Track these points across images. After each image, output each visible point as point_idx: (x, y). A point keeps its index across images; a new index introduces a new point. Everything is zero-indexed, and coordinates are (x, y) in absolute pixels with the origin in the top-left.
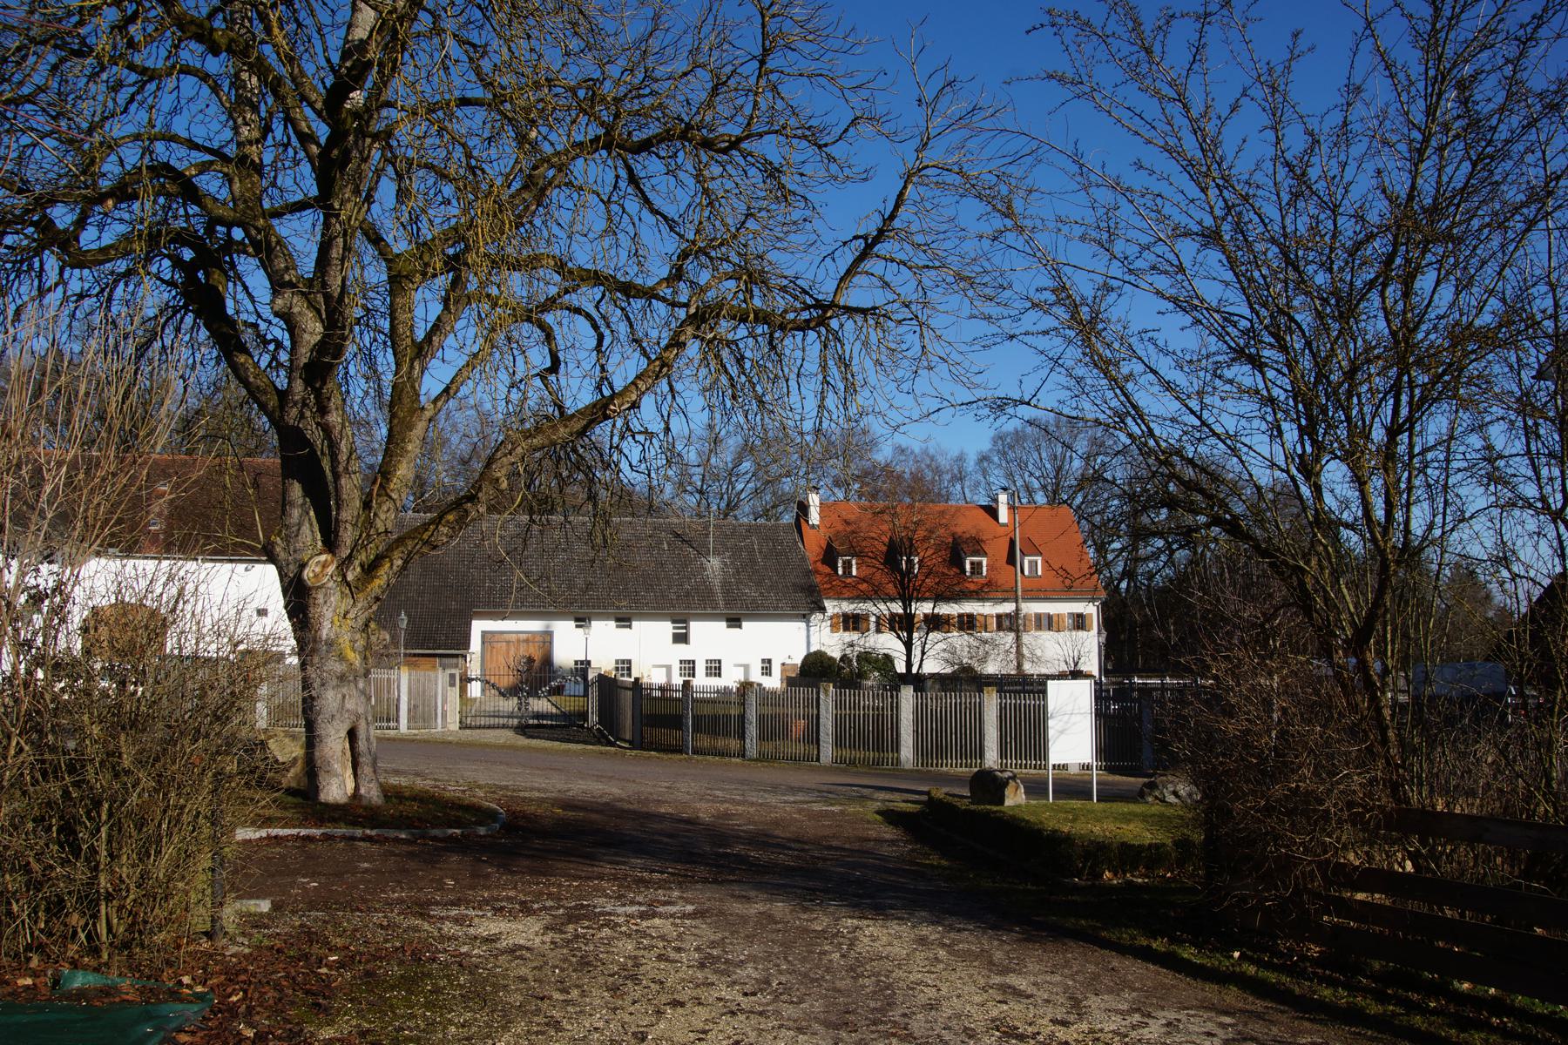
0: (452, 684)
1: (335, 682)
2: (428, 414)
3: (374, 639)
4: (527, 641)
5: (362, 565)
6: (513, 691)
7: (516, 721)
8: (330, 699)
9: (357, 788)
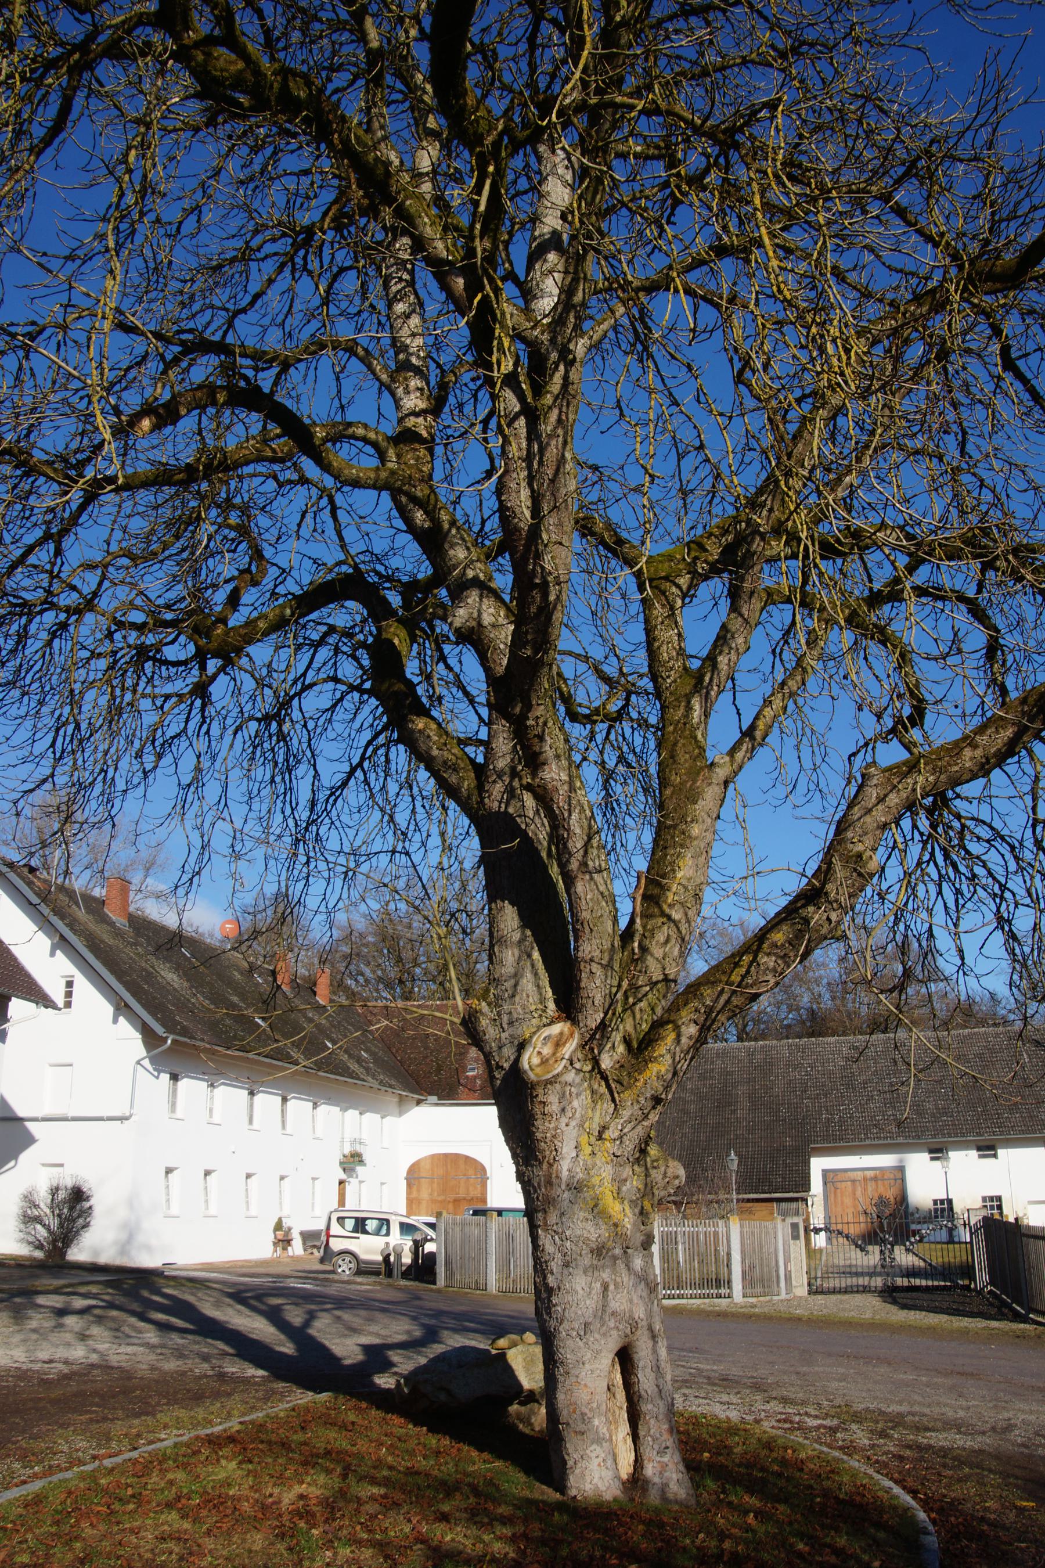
0: (796, 1237)
1: (587, 1260)
2: (721, 773)
3: (656, 1175)
4: (875, 1179)
5: (627, 1041)
6: (870, 1238)
7: (878, 1282)
8: (579, 1293)
9: (638, 1463)
